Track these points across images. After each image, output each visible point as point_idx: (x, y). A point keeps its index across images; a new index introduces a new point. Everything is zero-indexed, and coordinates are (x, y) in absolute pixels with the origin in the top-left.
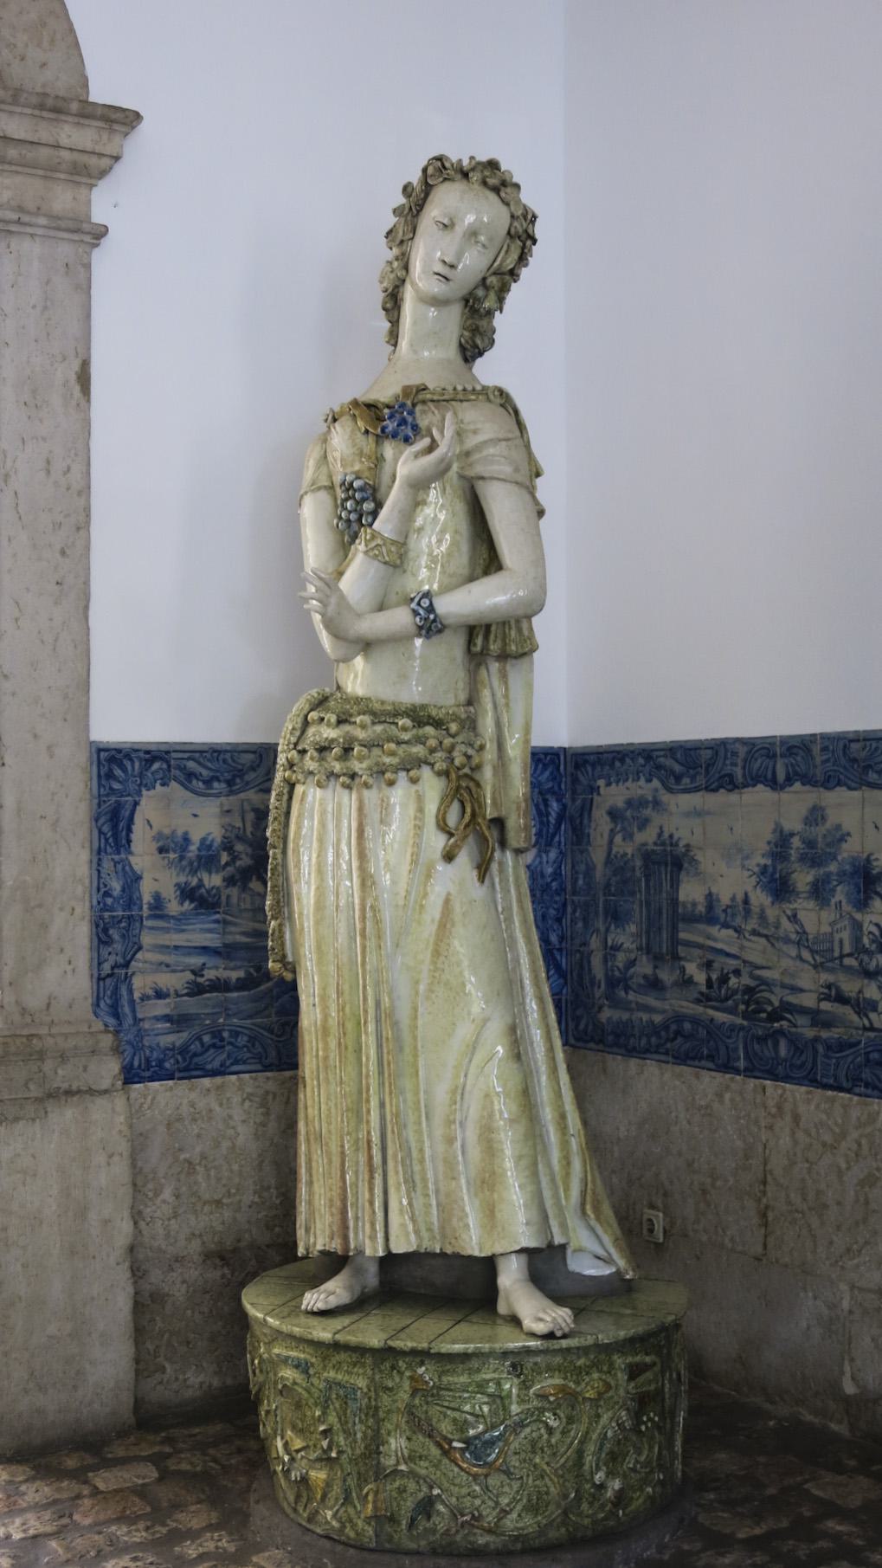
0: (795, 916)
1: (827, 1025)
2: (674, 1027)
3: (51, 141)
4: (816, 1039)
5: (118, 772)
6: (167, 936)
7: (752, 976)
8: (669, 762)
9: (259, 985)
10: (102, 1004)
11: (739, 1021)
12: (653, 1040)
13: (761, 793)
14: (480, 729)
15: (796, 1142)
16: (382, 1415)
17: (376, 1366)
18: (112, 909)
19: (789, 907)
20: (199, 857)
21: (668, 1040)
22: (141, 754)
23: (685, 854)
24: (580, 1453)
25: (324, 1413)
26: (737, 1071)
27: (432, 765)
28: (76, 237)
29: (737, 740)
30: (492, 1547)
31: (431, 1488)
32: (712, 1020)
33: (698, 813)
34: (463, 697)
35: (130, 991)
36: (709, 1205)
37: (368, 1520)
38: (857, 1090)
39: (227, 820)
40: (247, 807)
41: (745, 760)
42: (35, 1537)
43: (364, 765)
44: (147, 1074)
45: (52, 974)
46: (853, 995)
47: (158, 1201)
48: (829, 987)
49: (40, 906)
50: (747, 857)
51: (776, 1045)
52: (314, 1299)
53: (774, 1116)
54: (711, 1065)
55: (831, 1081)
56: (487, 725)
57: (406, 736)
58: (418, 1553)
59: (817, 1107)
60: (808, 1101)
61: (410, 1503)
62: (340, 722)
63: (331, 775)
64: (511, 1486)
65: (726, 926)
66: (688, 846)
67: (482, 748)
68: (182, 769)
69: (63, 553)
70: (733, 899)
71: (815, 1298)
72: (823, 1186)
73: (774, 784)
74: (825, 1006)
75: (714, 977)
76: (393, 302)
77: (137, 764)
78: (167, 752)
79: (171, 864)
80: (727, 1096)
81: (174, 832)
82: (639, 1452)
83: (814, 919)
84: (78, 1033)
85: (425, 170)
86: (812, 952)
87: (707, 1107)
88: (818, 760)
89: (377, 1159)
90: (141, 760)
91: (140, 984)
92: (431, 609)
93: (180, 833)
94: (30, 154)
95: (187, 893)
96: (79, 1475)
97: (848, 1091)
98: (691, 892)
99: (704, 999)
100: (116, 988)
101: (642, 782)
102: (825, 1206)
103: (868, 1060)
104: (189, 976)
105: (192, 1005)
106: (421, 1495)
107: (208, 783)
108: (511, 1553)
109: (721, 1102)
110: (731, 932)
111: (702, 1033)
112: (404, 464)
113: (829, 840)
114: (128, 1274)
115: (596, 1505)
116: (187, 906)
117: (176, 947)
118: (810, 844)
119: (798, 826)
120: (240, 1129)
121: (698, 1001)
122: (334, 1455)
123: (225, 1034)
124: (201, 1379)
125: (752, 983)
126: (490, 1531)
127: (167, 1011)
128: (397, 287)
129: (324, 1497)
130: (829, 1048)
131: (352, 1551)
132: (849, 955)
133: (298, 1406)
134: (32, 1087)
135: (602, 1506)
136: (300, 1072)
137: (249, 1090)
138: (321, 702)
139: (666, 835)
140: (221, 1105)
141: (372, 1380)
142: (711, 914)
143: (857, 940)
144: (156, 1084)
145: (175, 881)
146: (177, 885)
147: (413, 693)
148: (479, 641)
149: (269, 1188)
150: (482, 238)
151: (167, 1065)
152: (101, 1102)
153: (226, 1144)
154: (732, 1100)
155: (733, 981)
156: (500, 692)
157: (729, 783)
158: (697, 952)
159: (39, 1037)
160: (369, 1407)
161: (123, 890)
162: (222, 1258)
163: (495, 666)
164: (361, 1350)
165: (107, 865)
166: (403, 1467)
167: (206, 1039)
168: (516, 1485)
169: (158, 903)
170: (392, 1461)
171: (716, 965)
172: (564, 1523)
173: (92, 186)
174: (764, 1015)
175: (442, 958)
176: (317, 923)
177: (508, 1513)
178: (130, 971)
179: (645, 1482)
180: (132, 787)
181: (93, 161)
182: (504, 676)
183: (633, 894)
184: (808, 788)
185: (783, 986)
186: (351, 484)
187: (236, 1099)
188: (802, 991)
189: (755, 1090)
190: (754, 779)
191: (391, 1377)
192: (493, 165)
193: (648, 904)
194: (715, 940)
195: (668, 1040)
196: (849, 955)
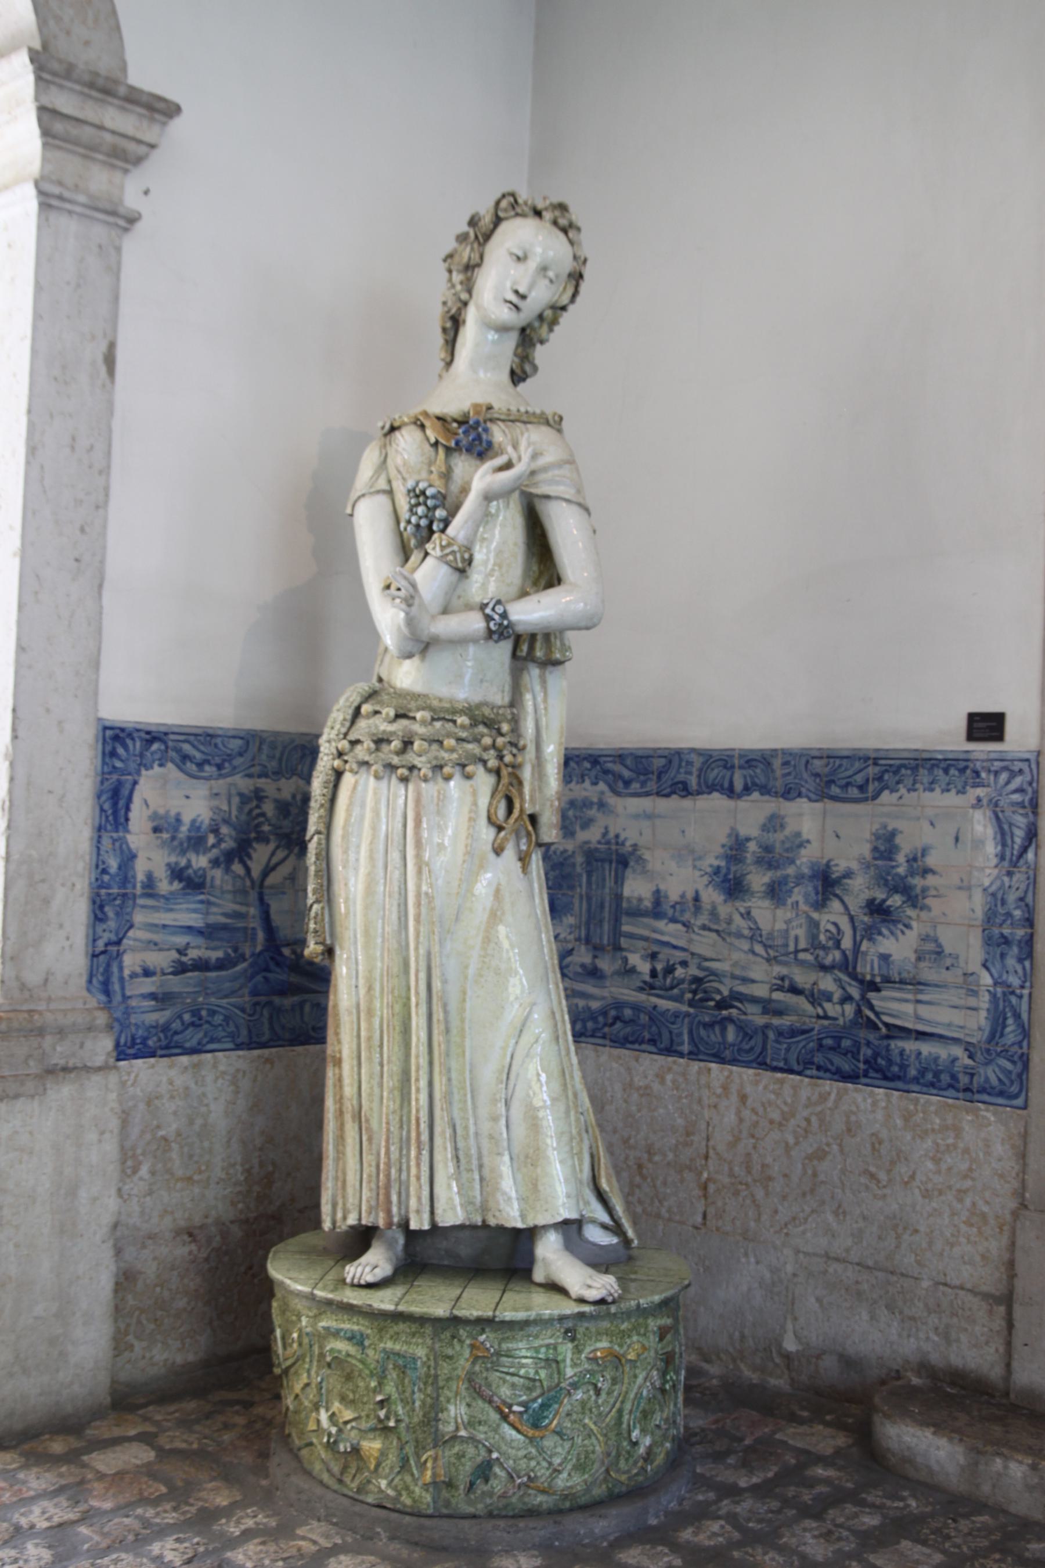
0: (749, 913)
1: (779, 1013)
2: (613, 1013)
3: (97, 121)
4: (767, 1026)
5: (120, 751)
6: (157, 915)
7: (700, 967)
8: (617, 768)
9: (235, 965)
10: (95, 981)
11: (685, 1008)
12: (590, 1025)
13: (717, 801)
14: (522, 730)
15: (741, 1120)
16: (441, 1384)
17: (435, 1336)
18: (108, 887)
19: (742, 906)
20: (189, 838)
21: (605, 1025)
22: (143, 735)
23: (632, 853)
24: (620, 1412)
25: (380, 1384)
26: (681, 1055)
27: (484, 762)
28: (111, 219)
29: (693, 750)
30: (545, 1506)
31: (490, 1452)
32: (655, 1007)
33: (649, 816)
34: (507, 700)
35: (121, 969)
36: (644, 1178)
37: (426, 1487)
38: (808, 1072)
39: (215, 803)
40: (234, 791)
41: (700, 770)
42: (60, 1525)
43: (423, 759)
44: (131, 1051)
45: (50, 949)
46: (808, 986)
47: (136, 1178)
48: (782, 979)
49: (43, 881)
50: (700, 858)
51: (724, 1030)
52: (354, 1271)
53: (719, 1096)
54: (652, 1049)
55: (781, 1064)
56: (529, 728)
57: (464, 734)
58: (474, 1517)
59: (765, 1088)
60: (757, 1083)
61: (468, 1467)
62: (398, 716)
63: (391, 767)
64: (562, 1446)
65: (673, 920)
66: (635, 845)
67: (524, 748)
68: (178, 751)
69: (82, 530)
70: (683, 896)
71: (757, 1263)
72: (769, 1160)
73: (730, 792)
74: (777, 996)
75: (659, 967)
76: (454, 323)
77: (138, 744)
78: (166, 734)
79: (164, 843)
80: (669, 1077)
81: (168, 812)
82: (662, 1411)
83: (767, 916)
84: (73, 1009)
85: (498, 203)
86: (766, 946)
87: (647, 1087)
88: (779, 773)
89: (425, 1137)
90: (141, 739)
91: (131, 961)
92: (504, 615)
93: (173, 813)
94: (74, 131)
95: (177, 873)
96: (72, 1457)
97: (799, 1073)
98: (636, 888)
99: (648, 987)
100: (108, 965)
101: (587, 784)
102: (770, 1178)
103: (821, 1046)
104: (174, 955)
105: (175, 984)
106: (479, 1459)
107: (200, 765)
108: (561, 1512)
109: (663, 1081)
110: (679, 926)
111: (644, 1018)
112: (482, 478)
113: (787, 845)
114: (112, 1253)
115: (631, 1461)
116: (177, 886)
117: (164, 926)
118: (768, 849)
119: (754, 832)
120: (213, 1107)
121: (641, 989)
122: (392, 1424)
123: (204, 1013)
124: (165, 1356)
125: (700, 974)
126: (543, 1492)
127: (153, 989)
128: (459, 310)
129: (378, 1465)
130: (780, 1034)
131: (408, 1518)
132: (805, 950)
133: (349, 1377)
134: (32, 1063)
135: (635, 1463)
136: (330, 1049)
137: (222, 1068)
138: (372, 695)
139: (611, 835)
140: (196, 1083)
141: (432, 1349)
142: (657, 908)
143: (813, 938)
144: (140, 1061)
145: (167, 860)
146: (168, 865)
147: (463, 693)
148: (525, 648)
149: (234, 1165)
150: (551, 274)
151: (150, 1043)
152: (97, 1078)
153: (199, 1121)
154: (674, 1081)
155: (680, 972)
156: (540, 698)
157: (684, 790)
158: (641, 944)
159: (40, 1013)
160: (428, 1376)
161: (120, 868)
162: (190, 1235)
163: (535, 671)
164: (422, 1320)
165: (106, 842)
166: (463, 1433)
167: (187, 1017)
168: (567, 1445)
169: (150, 882)
170: (451, 1428)
171: (660, 956)
172: (605, 1480)
173: (126, 171)
174: (712, 1003)
175: (492, 945)
176: (367, 907)
177: (559, 1472)
178: (122, 948)
179: (665, 1437)
180: (132, 766)
181: (131, 147)
182: (544, 682)
183: (572, 888)
184: (766, 797)
185: (734, 977)
186: (423, 493)
187: (209, 1079)
188: (753, 981)
189: (699, 1073)
190: (711, 788)
191: (452, 1345)
192: (562, 207)
193: (589, 898)
194: (662, 933)
195: (605, 1025)
196: (805, 950)
